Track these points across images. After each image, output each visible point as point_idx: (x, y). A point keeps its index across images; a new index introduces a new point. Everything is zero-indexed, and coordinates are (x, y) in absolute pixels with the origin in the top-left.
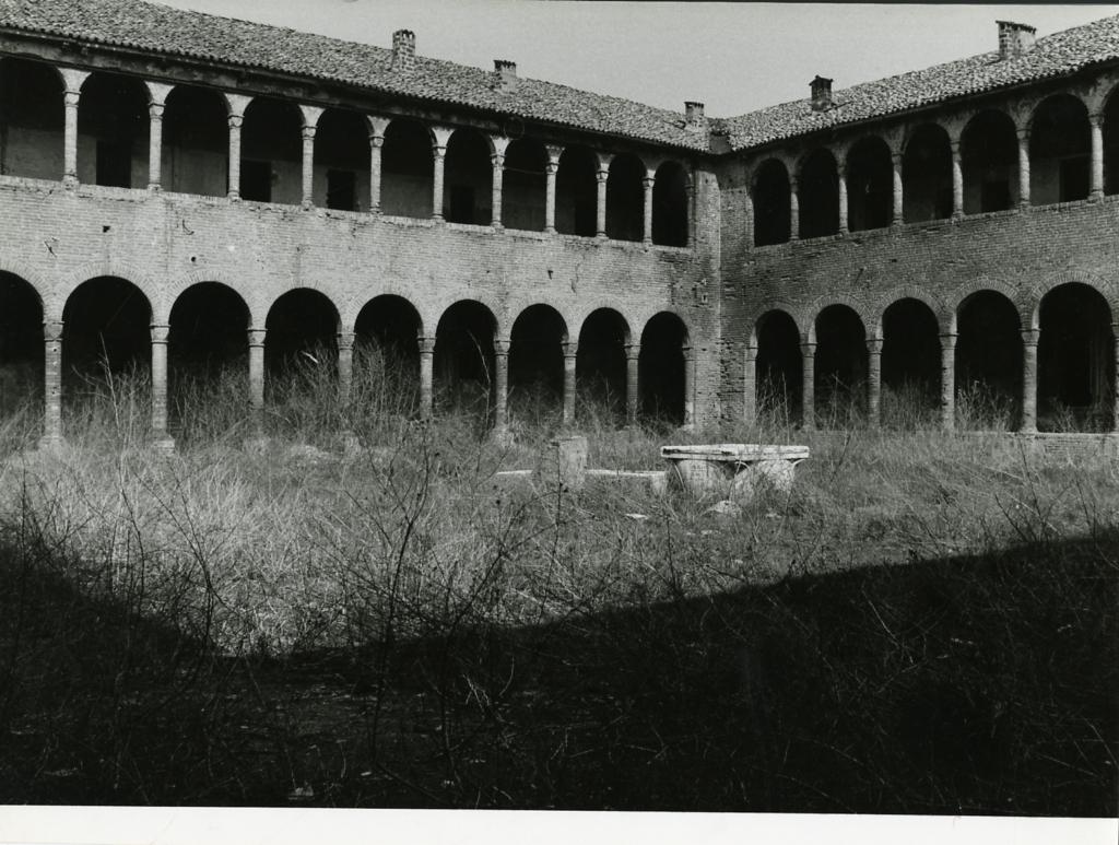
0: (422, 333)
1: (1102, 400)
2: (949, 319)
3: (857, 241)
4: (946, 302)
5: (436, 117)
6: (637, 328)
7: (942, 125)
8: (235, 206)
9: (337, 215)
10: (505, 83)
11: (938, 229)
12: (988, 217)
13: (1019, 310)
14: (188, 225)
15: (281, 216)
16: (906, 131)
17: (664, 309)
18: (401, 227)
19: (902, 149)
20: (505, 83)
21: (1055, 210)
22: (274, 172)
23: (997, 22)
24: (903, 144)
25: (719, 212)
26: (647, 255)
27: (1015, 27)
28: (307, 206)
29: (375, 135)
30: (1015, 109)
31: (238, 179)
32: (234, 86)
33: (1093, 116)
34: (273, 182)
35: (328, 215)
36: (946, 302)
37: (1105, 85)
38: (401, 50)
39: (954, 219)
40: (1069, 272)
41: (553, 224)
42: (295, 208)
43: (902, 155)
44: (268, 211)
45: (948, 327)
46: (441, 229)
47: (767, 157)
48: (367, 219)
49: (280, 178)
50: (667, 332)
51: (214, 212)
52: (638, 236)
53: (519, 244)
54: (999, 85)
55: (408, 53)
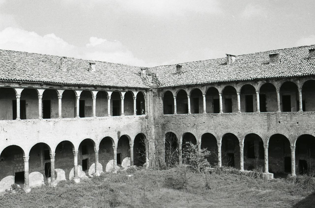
0: (74, 150)
1: (258, 158)
2: (220, 139)
3: (194, 116)
4: (219, 134)
5: (77, 88)
6: (133, 138)
7: (217, 88)
8: (19, 122)
9: (49, 120)
10: (92, 69)
11: (216, 116)
12: (230, 114)
13: (239, 139)
14: (5, 130)
15: (33, 123)
16: (207, 88)
17: (140, 133)
18: (68, 121)
19: (205, 93)
20: (92, 69)
21: (248, 114)
22: (27, 103)
23: (226, 54)
24: (206, 91)
25: (154, 106)
26: (135, 118)
27: (231, 56)
28: (40, 119)
29: (60, 95)
30: (236, 86)
31: (19, 113)
32: (18, 86)
33: (257, 91)
34: (26, 106)
35: (47, 121)
36: (219, 134)
37: (260, 83)
38: (63, 63)
39: (220, 113)
40: (252, 130)
41: (110, 114)
42: (37, 120)
43: (205, 95)
44: (29, 122)
45: (220, 142)
46: (79, 120)
47: (167, 90)
48: (58, 120)
49: (29, 105)
50: (140, 138)
51: (13, 125)
52: (132, 113)
53: (101, 121)
54: (232, 81)
55: (65, 63)
